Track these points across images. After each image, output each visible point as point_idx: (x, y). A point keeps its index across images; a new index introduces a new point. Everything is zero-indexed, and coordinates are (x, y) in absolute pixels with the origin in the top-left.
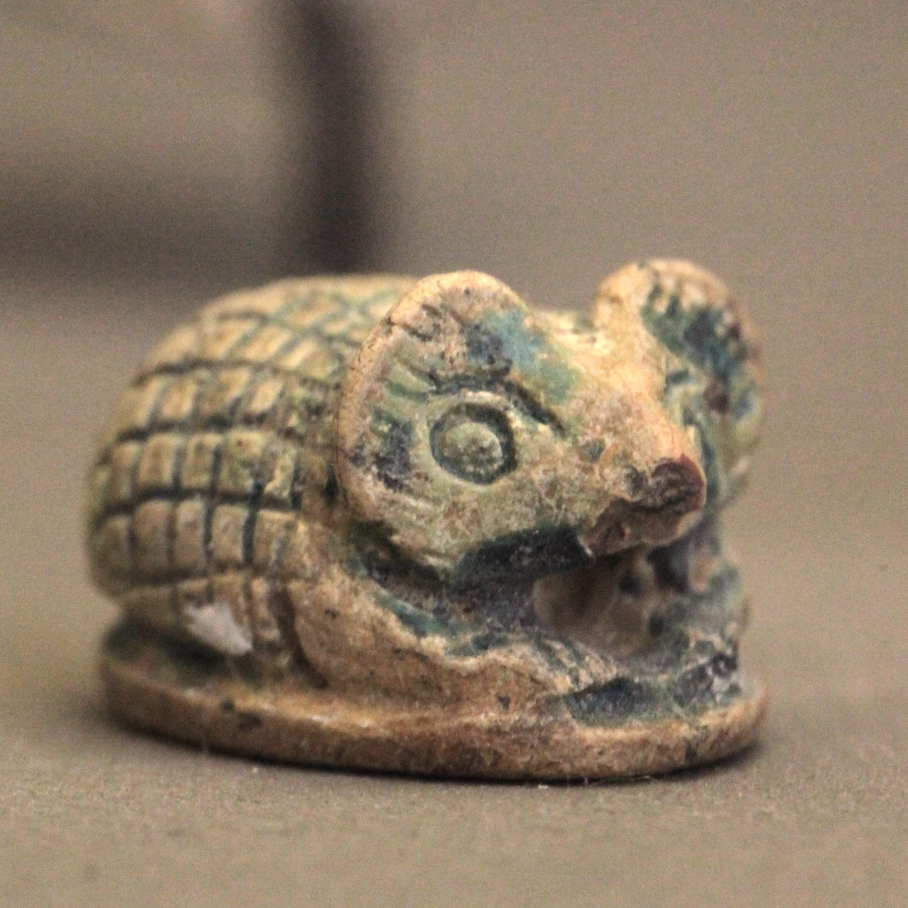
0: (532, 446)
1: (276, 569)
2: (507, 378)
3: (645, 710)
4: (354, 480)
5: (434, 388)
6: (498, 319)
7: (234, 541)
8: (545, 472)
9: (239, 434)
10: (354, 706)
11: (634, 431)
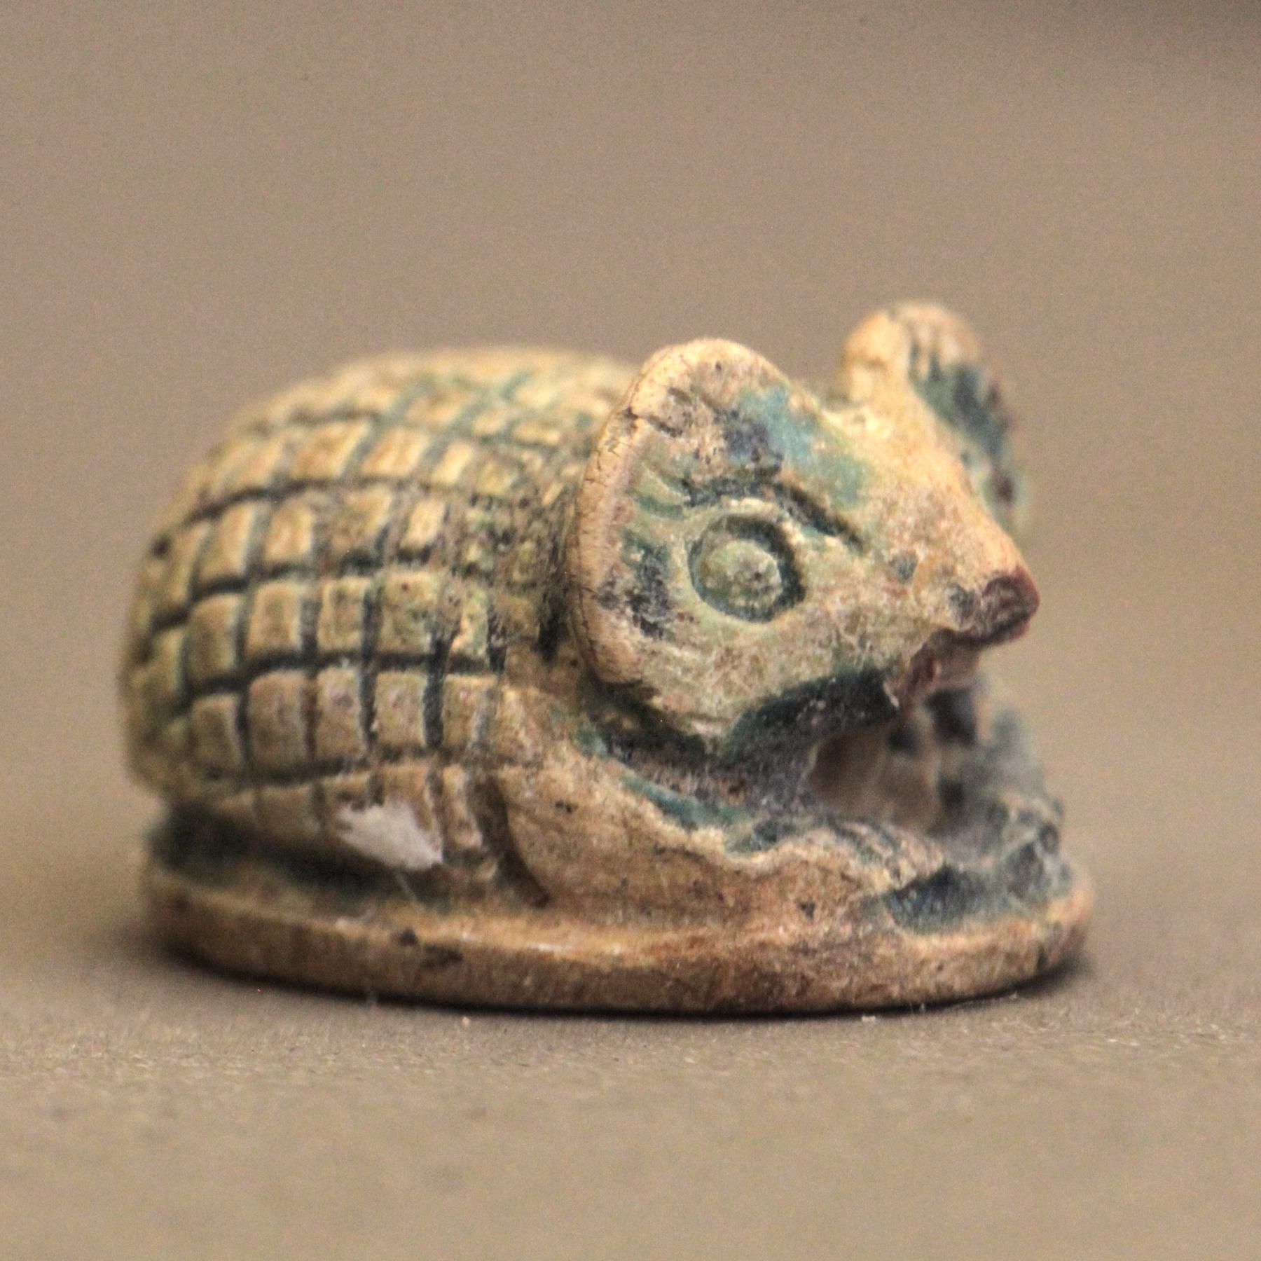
0: (822, 567)
1: (477, 752)
2: (776, 479)
3: (979, 906)
4: (605, 626)
5: (688, 498)
6: (758, 401)
7: (412, 720)
8: (843, 600)
9: (395, 576)
10: (593, 928)
11: (953, 537)
